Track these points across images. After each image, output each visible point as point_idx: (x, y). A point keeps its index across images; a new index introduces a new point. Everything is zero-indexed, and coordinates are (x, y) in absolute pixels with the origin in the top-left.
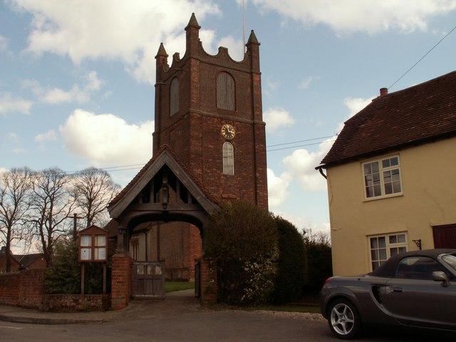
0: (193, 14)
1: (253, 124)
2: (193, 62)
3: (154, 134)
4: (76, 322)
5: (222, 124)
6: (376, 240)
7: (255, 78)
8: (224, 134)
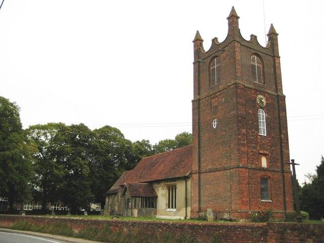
0: (198, 31)
5: (257, 95)
7: (277, 61)
8: (259, 102)
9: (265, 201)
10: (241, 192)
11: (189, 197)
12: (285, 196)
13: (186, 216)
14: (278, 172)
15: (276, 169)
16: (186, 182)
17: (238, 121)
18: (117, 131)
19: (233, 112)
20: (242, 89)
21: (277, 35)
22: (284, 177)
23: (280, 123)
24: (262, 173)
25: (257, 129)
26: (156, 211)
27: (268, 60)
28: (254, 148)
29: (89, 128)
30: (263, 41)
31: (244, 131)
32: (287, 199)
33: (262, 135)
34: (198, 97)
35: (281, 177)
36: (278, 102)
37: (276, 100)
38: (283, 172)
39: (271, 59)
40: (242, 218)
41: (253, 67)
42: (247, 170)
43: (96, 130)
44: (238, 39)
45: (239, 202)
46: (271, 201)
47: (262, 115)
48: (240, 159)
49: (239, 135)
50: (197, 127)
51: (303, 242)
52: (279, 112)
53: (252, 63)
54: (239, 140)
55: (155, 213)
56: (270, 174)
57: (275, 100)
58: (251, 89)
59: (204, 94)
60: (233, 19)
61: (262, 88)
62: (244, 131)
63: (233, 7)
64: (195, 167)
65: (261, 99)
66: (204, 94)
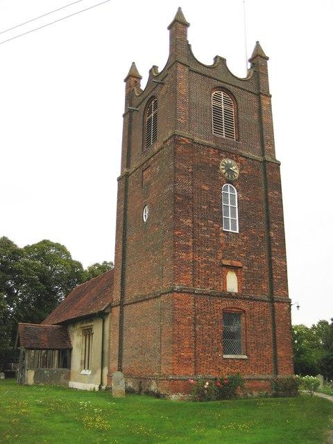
0: (134, 63)
5: (221, 158)
7: (264, 102)
8: (224, 171)
10: (176, 340)
11: (106, 349)
12: (275, 348)
13: (102, 384)
14: (263, 301)
15: (259, 296)
16: (104, 322)
17: (175, 203)
18: (61, 249)
19: (170, 188)
21: (267, 59)
22: (273, 311)
23: (267, 210)
25: (219, 220)
26: (70, 373)
27: (245, 99)
28: (211, 254)
29: (16, 242)
30: (239, 68)
31: (188, 222)
32: (280, 353)
33: (230, 230)
34: (126, 170)
35: (268, 313)
36: (265, 174)
38: (272, 301)
39: (254, 98)
40: (176, 391)
41: (217, 110)
42: (192, 297)
43: (27, 248)
44: (184, 60)
45: (170, 359)
46: (245, 357)
47: (231, 197)
48: (176, 276)
49: (175, 229)
50: (122, 223)
51: (320, 443)
52: (266, 192)
53: (217, 104)
54: (176, 237)
55: (68, 377)
56: (244, 305)
58: (209, 147)
59: (134, 165)
60: (179, 27)
62: (188, 222)
63: (180, 8)
64: (116, 296)
65: (228, 167)
66: (134, 165)
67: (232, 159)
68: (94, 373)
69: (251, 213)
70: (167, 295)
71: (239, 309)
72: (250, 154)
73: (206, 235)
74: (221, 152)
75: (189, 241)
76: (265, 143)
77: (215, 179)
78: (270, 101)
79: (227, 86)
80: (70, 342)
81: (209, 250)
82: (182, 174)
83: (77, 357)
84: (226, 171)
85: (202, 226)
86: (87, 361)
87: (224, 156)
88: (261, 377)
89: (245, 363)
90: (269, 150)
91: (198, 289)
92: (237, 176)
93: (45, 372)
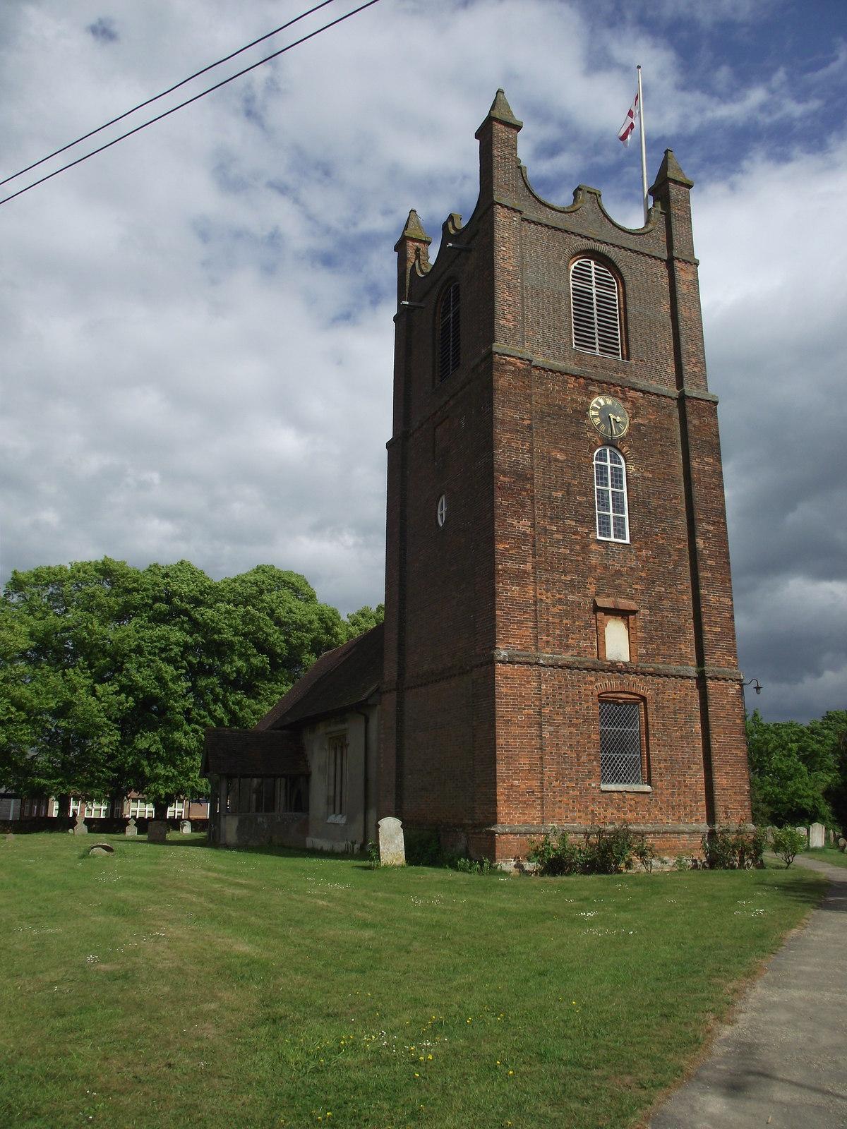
0: (499, 92)
1: (682, 400)
2: (501, 216)
3: (390, 445)
4: (341, 797)
5: (591, 395)
6: (827, 712)
7: (682, 275)
8: (597, 421)
9: (621, 787)
15: (674, 668)
16: (367, 721)
20: (517, 373)
24: (610, 683)
28: (571, 585)
33: (612, 539)
37: (676, 413)
41: (582, 298)
42: (533, 671)
46: (647, 788)
47: (614, 479)
55: (305, 829)
57: (670, 415)
61: (616, 370)
67: (614, 395)
68: (351, 820)
69: (655, 502)
70: (483, 669)
71: (635, 694)
72: (654, 385)
73: (562, 550)
74: (590, 384)
75: (525, 562)
76: (684, 361)
77: (577, 437)
78: (696, 274)
79: (603, 248)
80: (306, 761)
81: (568, 578)
82: (510, 431)
83: (319, 790)
84: (603, 421)
85: (552, 532)
86: (338, 798)
87: (597, 390)
88: (682, 827)
89: (647, 800)
90: (694, 375)
91: (546, 656)
92: (625, 431)
93: (260, 819)
